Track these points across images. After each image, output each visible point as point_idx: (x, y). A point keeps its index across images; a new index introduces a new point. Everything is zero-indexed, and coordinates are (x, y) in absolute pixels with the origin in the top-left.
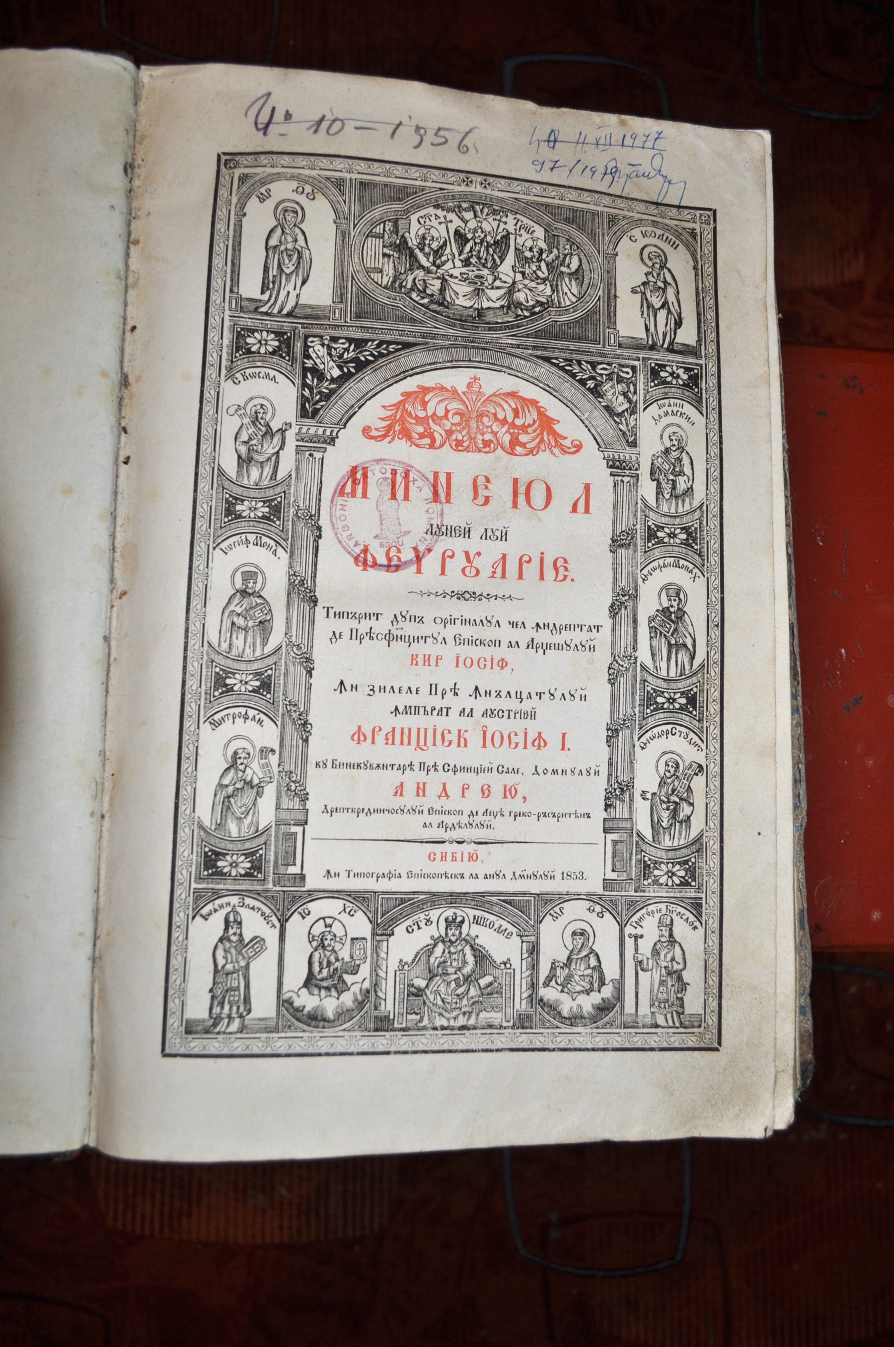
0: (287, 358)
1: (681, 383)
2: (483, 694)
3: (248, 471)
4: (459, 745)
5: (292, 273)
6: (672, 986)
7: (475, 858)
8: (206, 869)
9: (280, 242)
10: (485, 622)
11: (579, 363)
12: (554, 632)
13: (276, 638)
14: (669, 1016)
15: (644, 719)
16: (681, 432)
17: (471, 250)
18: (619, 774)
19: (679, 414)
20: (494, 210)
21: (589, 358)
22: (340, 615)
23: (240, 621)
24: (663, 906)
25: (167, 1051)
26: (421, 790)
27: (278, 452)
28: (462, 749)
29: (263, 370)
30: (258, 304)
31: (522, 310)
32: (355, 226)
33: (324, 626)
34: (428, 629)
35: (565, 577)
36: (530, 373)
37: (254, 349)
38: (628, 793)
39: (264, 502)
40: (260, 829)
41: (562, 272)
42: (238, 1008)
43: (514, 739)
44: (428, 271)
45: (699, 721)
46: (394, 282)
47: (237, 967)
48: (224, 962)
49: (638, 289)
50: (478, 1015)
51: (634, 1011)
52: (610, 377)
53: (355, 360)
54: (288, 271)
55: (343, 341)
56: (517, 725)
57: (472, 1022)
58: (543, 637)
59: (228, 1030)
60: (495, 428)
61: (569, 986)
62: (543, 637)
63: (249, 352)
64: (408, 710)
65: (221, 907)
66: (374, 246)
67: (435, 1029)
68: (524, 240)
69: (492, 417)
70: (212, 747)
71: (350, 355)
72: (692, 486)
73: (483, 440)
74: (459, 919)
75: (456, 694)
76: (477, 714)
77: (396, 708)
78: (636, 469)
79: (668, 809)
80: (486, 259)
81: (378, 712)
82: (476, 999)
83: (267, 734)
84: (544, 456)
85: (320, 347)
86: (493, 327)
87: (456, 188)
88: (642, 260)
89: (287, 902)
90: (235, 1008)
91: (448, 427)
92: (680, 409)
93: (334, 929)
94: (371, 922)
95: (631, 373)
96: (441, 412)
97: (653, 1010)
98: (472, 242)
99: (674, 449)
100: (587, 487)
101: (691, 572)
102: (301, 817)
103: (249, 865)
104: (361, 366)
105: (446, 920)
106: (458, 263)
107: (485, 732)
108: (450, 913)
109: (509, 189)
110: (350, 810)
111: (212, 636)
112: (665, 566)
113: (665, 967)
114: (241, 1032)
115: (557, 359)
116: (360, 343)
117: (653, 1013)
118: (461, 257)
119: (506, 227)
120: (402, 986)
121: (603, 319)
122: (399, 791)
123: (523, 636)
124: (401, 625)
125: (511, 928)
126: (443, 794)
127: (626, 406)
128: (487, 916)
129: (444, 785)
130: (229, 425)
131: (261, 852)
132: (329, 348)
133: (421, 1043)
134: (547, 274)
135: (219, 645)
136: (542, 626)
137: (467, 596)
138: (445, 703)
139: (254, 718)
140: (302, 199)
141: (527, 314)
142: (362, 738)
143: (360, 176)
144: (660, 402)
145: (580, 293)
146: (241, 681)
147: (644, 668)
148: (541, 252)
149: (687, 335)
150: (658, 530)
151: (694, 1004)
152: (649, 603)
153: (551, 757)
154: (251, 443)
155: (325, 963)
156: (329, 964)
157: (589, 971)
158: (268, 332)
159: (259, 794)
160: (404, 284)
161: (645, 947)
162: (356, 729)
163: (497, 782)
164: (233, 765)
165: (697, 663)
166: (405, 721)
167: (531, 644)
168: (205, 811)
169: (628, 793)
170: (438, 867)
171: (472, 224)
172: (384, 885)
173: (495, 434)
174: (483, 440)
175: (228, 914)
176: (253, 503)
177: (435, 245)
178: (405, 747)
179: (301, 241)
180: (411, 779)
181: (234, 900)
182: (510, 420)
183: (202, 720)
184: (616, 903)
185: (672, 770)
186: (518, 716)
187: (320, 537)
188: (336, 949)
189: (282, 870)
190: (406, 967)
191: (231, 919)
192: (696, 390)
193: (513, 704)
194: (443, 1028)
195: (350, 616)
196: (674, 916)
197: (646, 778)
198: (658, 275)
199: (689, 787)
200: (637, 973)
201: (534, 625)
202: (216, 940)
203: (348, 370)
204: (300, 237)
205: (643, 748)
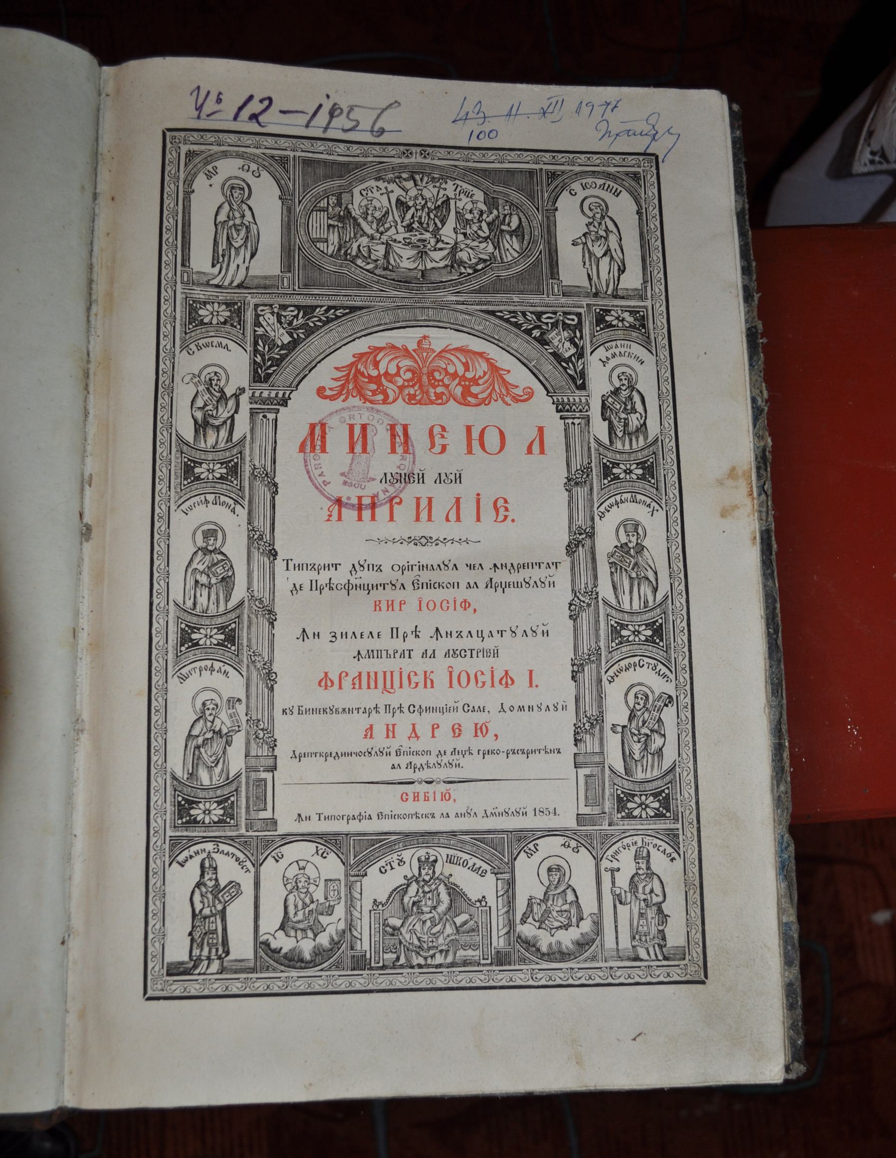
1: (627, 325)
2: (444, 635)
3: (204, 436)
4: (425, 687)
5: (240, 247)
7: (447, 798)
9: (228, 217)
10: (442, 566)
11: (524, 314)
12: (512, 571)
13: (239, 593)
15: (610, 652)
17: (413, 217)
18: (587, 708)
19: (627, 354)
20: (434, 178)
21: (532, 309)
22: (300, 567)
23: (203, 579)
24: (638, 839)
25: (150, 993)
26: (391, 731)
27: (232, 417)
28: (429, 690)
29: (215, 340)
31: (465, 268)
32: (300, 202)
33: (284, 579)
34: (387, 575)
37: (206, 320)
39: (222, 464)
40: (231, 776)
41: (502, 231)
42: (217, 950)
43: (481, 678)
46: (339, 249)
47: (214, 912)
49: (579, 241)
50: (455, 954)
51: (615, 946)
52: (555, 325)
53: (304, 326)
54: (237, 245)
55: (292, 308)
56: (483, 664)
58: (502, 576)
59: (209, 971)
60: (446, 381)
62: (502, 576)
63: (202, 323)
64: (370, 654)
65: (197, 853)
66: (318, 221)
67: (412, 967)
68: (464, 203)
70: (183, 700)
71: (300, 322)
72: (645, 423)
74: (432, 859)
75: (417, 636)
76: (440, 654)
78: (587, 411)
79: (639, 742)
80: (428, 224)
81: (339, 658)
82: (453, 937)
83: (232, 685)
84: (496, 406)
85: (270, 316)
86: (440, 285)
87: (397, 161)
88: (582, 211)
89: (260, 847)
90: (214, 951)
93: (307, 871)
94: (344, 864)
95: (576, 319)
96: (392, 370)
97: (634, 943)
99: (624, 388)
100: (541, 430)
101: (649, 506)
102: (270, 762)
103: (222, 812)
104: (310, 331)
105: (419, 860)
107: (451, 673)
108: (422, 853)
109: (449, 157)
110: (318, 755)
111: (177, 593)
112: (622, 502)
113: (644, 900)
114: (221, 973)
115: (501, 312)
116: (308, 310)
117: (634, 947)
118: (404, 224)
119: (446, 192)
120: (377, 926)
122: (369, 732)
123: (482, 578)
124: (359, 574)
125: (485, 866)
126: (413, 735)
127: (573, 351)
128: (460, 854)
129: (414, 725)
130: (184, 393)
132: (279, 316)
133: (399, 982)
134: (488, 233)
135: (184, 603)
136: (499, 566)
137: (424, 541)
138: (407, 645)
139: (219, 671)
141: (470, 271)
142: (329, 684)
143: (303, 154)
144: (606, 345)
145: (521, 248)
146: (206, 636)
147: (606, 603)
148: (481, 213)
150: (613, 467)
151: (676, 937)
152: (606, 538)
153: (520, 693)
154: (207, 408)
155: (300, 907)
157: (566, 907)
158: (219, 303)
159: (229, 743)
160: (349, 251)
162: (323, 675)
163: (468, 721)
165: (660, 596)
167: (490, 583)
168: (177, 763)
170: (410, 807)
171: (413, 192)
172: (355, 827)
173: (447, 386)
174: (435, 393)
175: (204, 860)
177: (378, 214)
178: (372, 691)
179: (248, 217)
180: (380, 721)
181: (209, 846)
184: (586, 836)
185: (642, 702)
186: (480, 654)
187: (276, 492)
188: (311, 890)
189: (253, 815)
190: (380, 906)
191: (207, 865)
192: (643, 330)
193: (475, 643)
194: (420, 966)
195: (309, 567)
196: (651, 848)
197: (617, 713)
198: (600, 224)
200: (615, 907)
203: (298, 335)
204: (248, 213)
205: (610, 682)
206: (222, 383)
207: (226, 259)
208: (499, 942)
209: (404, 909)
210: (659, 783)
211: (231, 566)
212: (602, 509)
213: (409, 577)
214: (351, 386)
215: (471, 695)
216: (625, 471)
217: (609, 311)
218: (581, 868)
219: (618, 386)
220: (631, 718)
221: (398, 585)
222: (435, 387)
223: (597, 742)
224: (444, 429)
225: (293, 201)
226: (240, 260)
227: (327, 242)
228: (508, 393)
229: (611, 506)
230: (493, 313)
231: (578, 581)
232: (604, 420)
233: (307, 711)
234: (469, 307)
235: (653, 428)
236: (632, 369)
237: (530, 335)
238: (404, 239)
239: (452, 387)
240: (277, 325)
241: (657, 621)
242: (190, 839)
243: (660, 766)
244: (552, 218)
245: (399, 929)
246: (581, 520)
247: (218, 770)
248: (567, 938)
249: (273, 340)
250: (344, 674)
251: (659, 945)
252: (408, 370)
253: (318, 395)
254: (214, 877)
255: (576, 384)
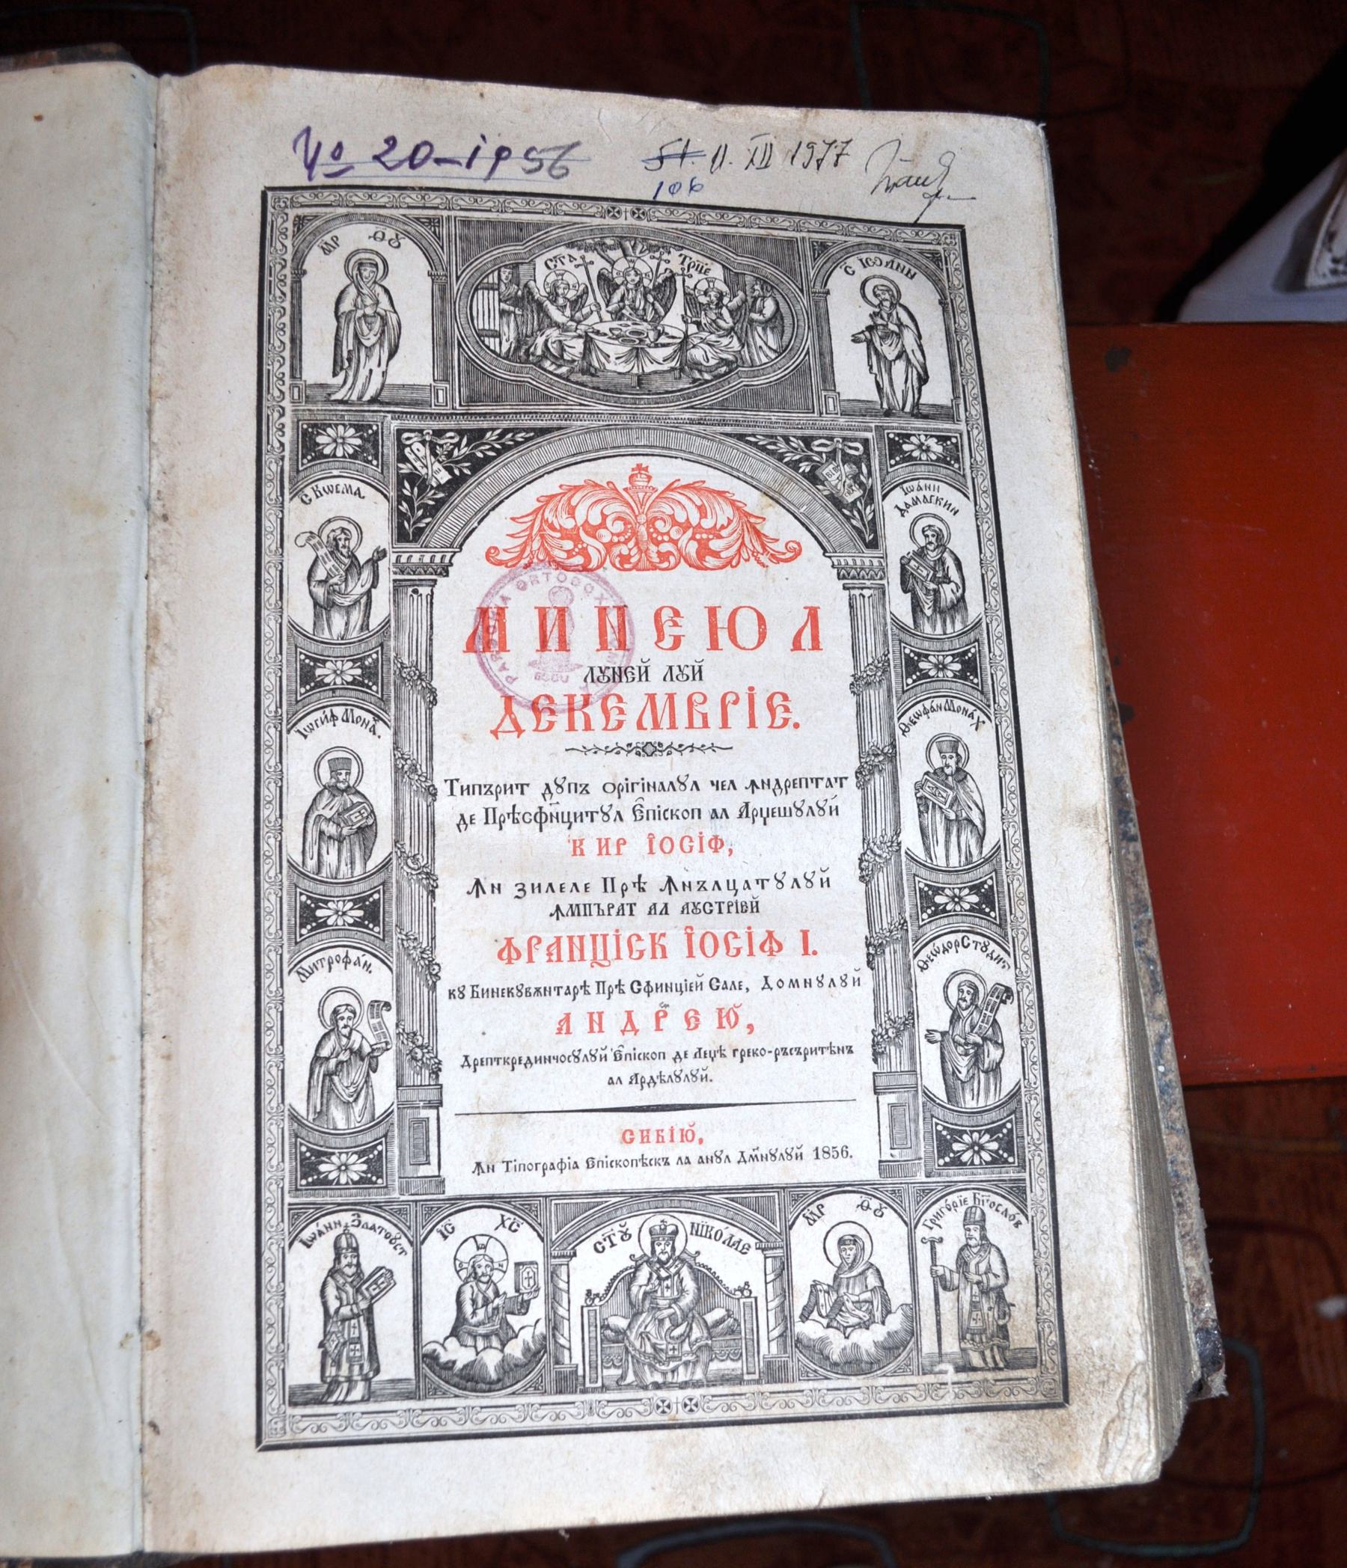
0: (375, 462)
1: (934, 457)
4: (654, 957)
6: (990, 1309)
8: (304, 1176)
10: (677, 785)
11: (787, 440)
12: (778, 791)
13: (382, 848)
14: (988, 1353)
16: (938, 524)
17: (622, 299)
21: (799, 433)
22: (468, 790)
23: (331, 829)
24: (969, 1195)
27: (369, 593)
28: (659, 961)
30: (329, 391)
31: (700, 371)
32: (458, 278)
33: (446, 808)
34: (596, 800)
35: (786, 721)
36: (718, 457)
37: (327, 451)
38: (906, 1034)
39: (354, 661)
41: (751, 321)
42: (361, 1367)
43: (734, 944)
44: (563, 328)
45: (1000, 926)
46: (518, 348)
48: (337, 1304)
49: (862, 336)
50: (707, 1366)
52: (832, 455)
55: (451, 434)
56: (739, 923)
57: (699, 1375)
58: (763, 799)
59: (349, 1399)
60: (674, 535)
61: (839, 1318)
62: (763, 799)
65: (329, 1227)
66: (486, 303)
67: (645, 1388)
69: (669, 520)
72: (963, 596)
73: (659, 552)
74: (670, 1229)
76: (675, 909)
77: (558, 908)
79: (966, 1055)
82: (703, 1343)
83: (376, 983)
84: (749, 569)
86: (664, 396)
87: (597, 221)
88: (864, 296)
91: (607, 539)
92: (936, 494)
94: (542, 1240)
96: (595, 519)
98: (622, 288)
99: (931, 547)
101: (971, 716)
102: (432, 1095)
103: (364, 1167)
104: (478, 465)
105: (651, 1232)
106: (607, 317)
107: (689, 936)
108: (655, 1221)
111: (293, 849)
113: (978, 1283)
115: (754, 436)
117: (963, 1350)
118: (610, 308)
119: (668, 266)
121: (815, 379)
123: (732, 801)
124: (556, 798)
125: (748, 1239)
128: (711, 1222)
129: (629, 1013)
130: (297, 562)
131: (379, 1148)
136: (759, 784)
140: (382, 247)
141: (707, 377)
142: (514, 955)
144: (905, 486)
146: (337, 912)
149: (938, 392)
151: (1022, 1336)
152: (913, 766)
154: (331, 581)
155: (480, 1302)
156: (486, 1302)
157: (867, 1296)
161: (947, 1256)
163: (707, 1002)
164: (334, 1029)
165: (987, 850)
166: (570, 926)
167: (745, 811)
169: (906, 1034)
173: (675, 542)
174: (659, 552)
175: (338, 1238)
176: (339, 664)
179: (384, 303)
181: (346, 1218)
182: (694, 521)
183: (286, 970)
185: (968, 998)
186: (733, 909)
187: (434, 702)
188: (495, 1278)
189: (409, 1170)
190: (597, 1300)
191: (344, 1243)
195: (484, 790)
196: (986, 1208)
197: (934, 1015)
198: (890, 315)
199: (995, 1021)
200: (936, 1295)
201: (748, 784)
202: (326, 1273)
203: (461, 471)
206: (352, 544)
207: (353, 365)
208: (769, 1349)
209: (631, 1303)
210: (994, 1115)
211: (372, 811)
212: (905, 719)
213: (629, 800)
214: (536, 545)
215: (722, 967)
216: (936, 666)
217: (908, 436)
218: (886, 1237)
219: (923, 544)
220: (955, 1018)
221: (613, 814)
222: (658, 543)
223: (906, 1056)
224: (677, 613)
225: (448, 276)
226: (373, 363)
227: (499, 336)
228: (764, 549)
229: (918, 716)
230: (741, 437)
231: (872, 827)
232: (905, 591)
233: (485, 993)
234: (708, 428)
235: (975, 608)
236: (942, 520)
237: (796, 468)
238: (611, 330)
239: (682, 543)
240: (430, 459)
241: (985, 882)
242: (318, 1206)
243: (998, 1089)
244: (821, 304)
245: (624, 1333)
246: (877, 738)
247: (358, 1107)
248: (867, 1340)
249: (425, 480)
250: (534, 941)
251: (998, 1347)
252: (619, 518)
253: (488, 560)
254: (355, 1261)
255: (863, 540)
